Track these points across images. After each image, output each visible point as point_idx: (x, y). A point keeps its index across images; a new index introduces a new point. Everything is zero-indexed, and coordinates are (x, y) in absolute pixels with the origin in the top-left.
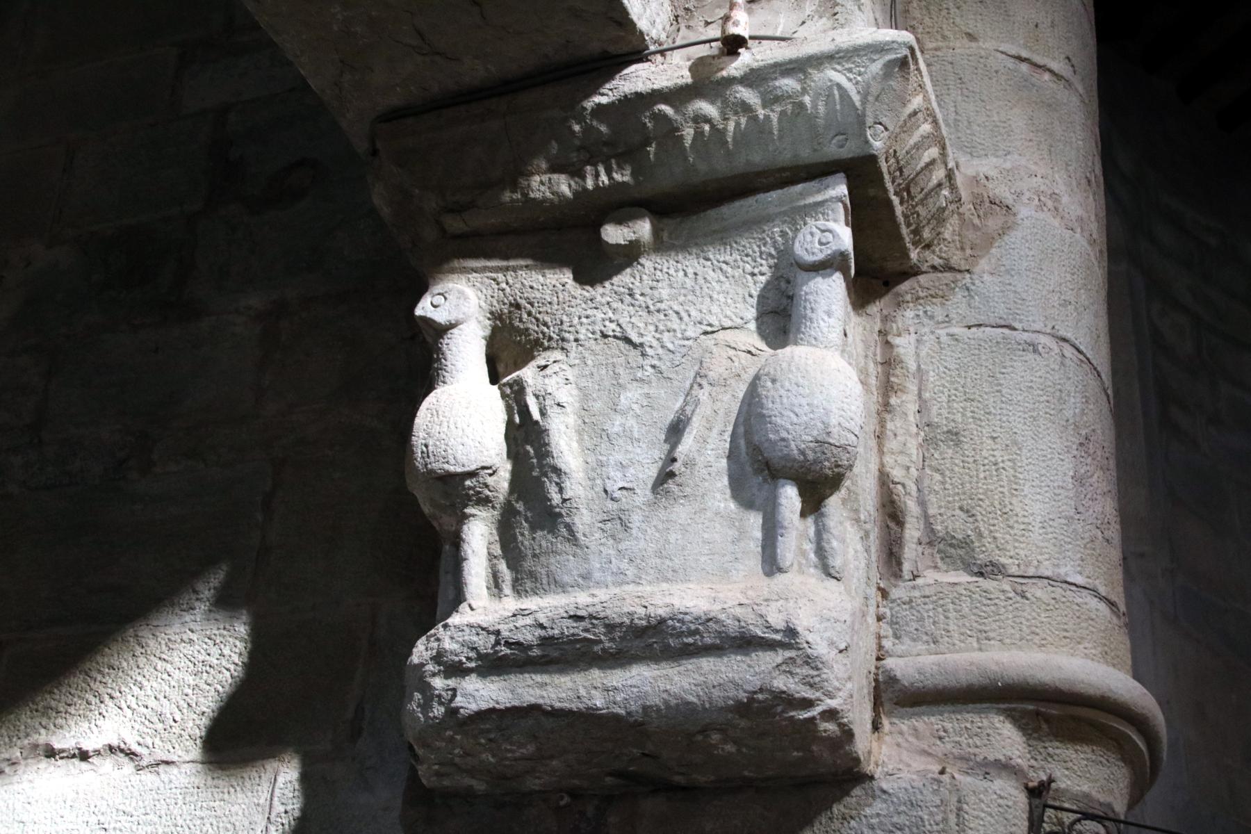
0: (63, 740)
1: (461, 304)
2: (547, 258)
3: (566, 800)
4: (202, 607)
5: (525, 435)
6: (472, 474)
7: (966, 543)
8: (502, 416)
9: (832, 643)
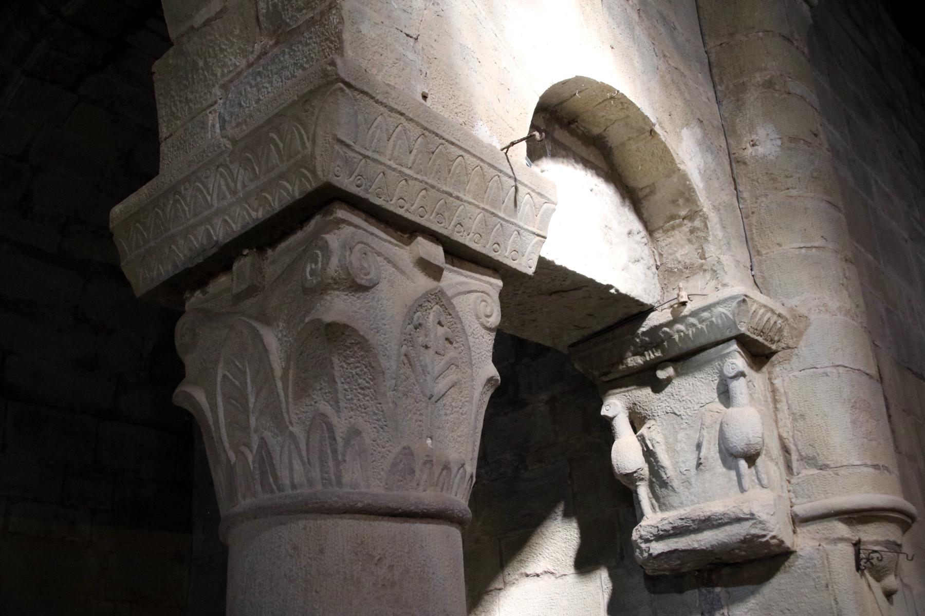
0: (529, 571)
1: (615, 407)
2: (641, 384)
3: (697, 573)
4: (560, 518)
5: (649, 454)
6: (635, 472)
7: (814, 458)
8: (640, 448)
9: (768, 514)
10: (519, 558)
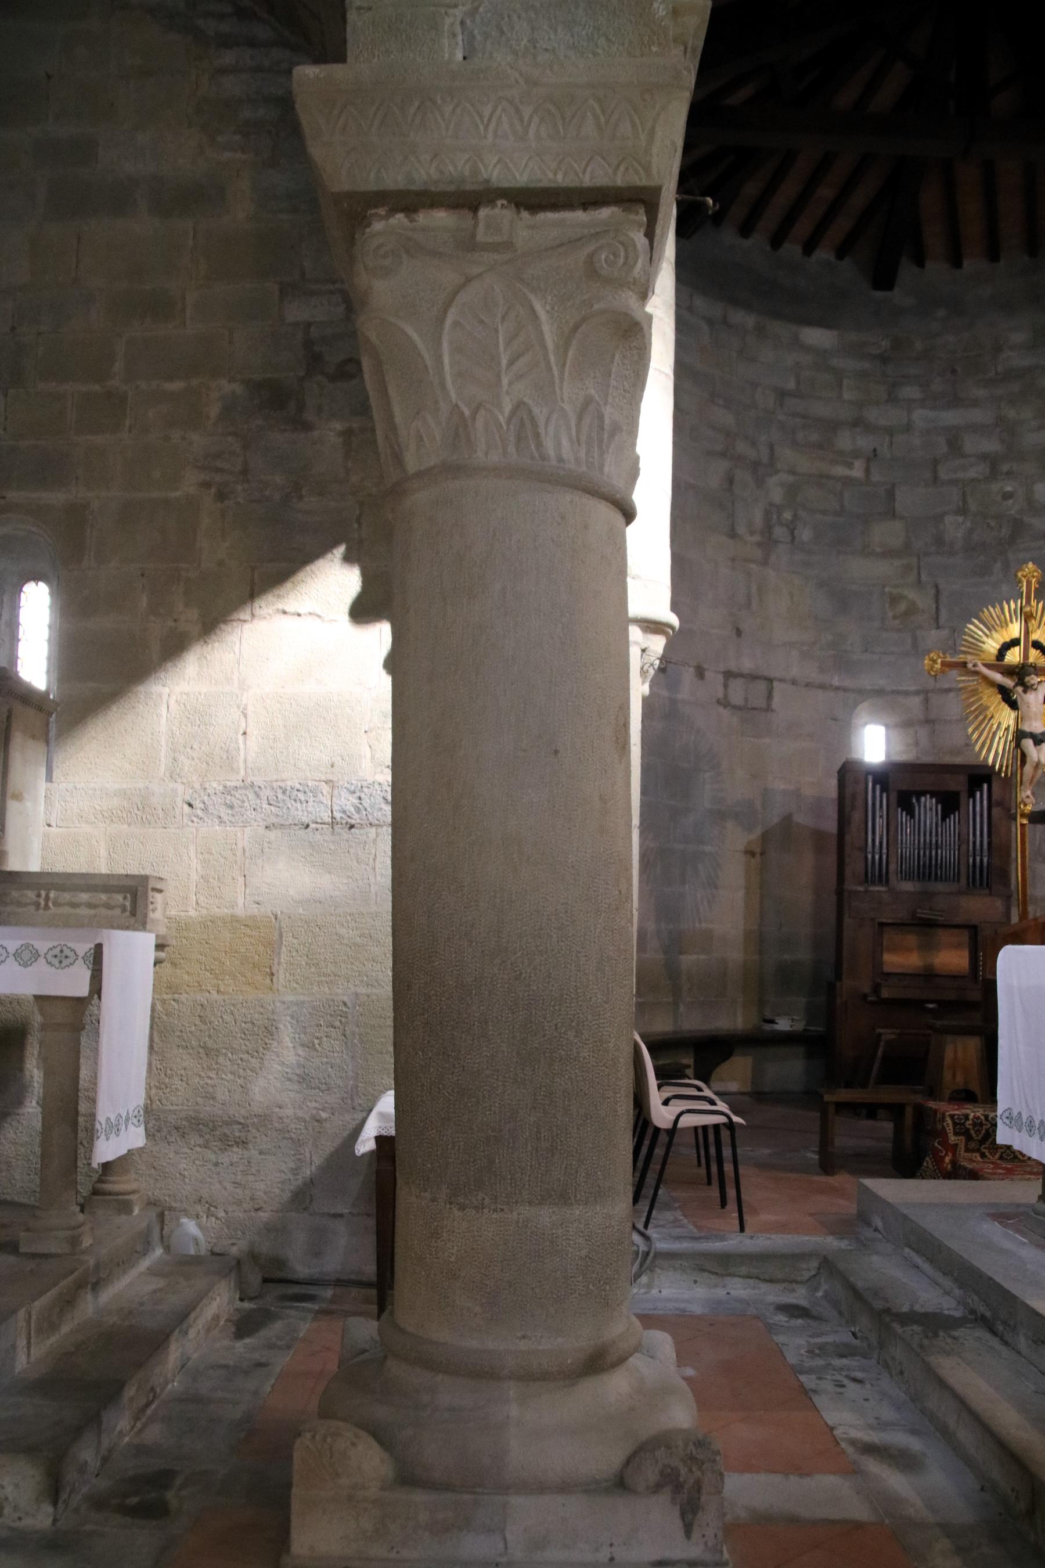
10: (276, 592)
